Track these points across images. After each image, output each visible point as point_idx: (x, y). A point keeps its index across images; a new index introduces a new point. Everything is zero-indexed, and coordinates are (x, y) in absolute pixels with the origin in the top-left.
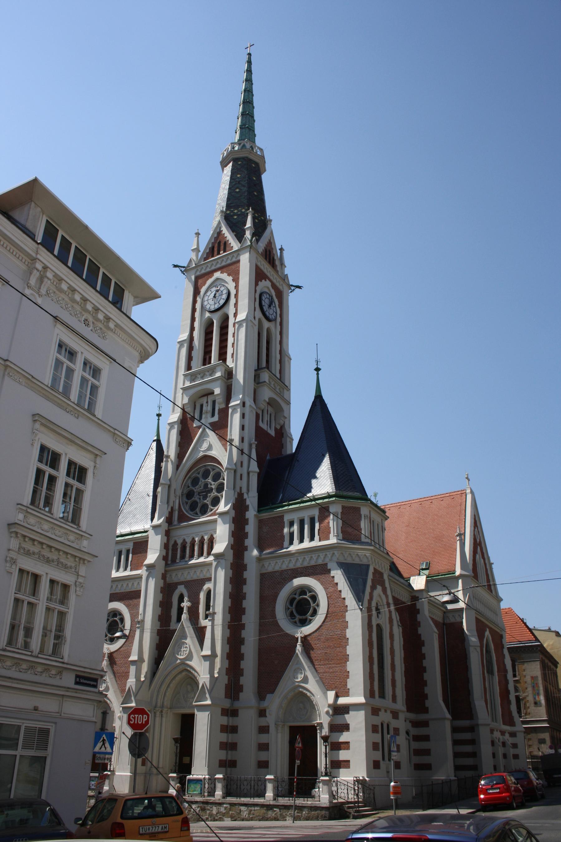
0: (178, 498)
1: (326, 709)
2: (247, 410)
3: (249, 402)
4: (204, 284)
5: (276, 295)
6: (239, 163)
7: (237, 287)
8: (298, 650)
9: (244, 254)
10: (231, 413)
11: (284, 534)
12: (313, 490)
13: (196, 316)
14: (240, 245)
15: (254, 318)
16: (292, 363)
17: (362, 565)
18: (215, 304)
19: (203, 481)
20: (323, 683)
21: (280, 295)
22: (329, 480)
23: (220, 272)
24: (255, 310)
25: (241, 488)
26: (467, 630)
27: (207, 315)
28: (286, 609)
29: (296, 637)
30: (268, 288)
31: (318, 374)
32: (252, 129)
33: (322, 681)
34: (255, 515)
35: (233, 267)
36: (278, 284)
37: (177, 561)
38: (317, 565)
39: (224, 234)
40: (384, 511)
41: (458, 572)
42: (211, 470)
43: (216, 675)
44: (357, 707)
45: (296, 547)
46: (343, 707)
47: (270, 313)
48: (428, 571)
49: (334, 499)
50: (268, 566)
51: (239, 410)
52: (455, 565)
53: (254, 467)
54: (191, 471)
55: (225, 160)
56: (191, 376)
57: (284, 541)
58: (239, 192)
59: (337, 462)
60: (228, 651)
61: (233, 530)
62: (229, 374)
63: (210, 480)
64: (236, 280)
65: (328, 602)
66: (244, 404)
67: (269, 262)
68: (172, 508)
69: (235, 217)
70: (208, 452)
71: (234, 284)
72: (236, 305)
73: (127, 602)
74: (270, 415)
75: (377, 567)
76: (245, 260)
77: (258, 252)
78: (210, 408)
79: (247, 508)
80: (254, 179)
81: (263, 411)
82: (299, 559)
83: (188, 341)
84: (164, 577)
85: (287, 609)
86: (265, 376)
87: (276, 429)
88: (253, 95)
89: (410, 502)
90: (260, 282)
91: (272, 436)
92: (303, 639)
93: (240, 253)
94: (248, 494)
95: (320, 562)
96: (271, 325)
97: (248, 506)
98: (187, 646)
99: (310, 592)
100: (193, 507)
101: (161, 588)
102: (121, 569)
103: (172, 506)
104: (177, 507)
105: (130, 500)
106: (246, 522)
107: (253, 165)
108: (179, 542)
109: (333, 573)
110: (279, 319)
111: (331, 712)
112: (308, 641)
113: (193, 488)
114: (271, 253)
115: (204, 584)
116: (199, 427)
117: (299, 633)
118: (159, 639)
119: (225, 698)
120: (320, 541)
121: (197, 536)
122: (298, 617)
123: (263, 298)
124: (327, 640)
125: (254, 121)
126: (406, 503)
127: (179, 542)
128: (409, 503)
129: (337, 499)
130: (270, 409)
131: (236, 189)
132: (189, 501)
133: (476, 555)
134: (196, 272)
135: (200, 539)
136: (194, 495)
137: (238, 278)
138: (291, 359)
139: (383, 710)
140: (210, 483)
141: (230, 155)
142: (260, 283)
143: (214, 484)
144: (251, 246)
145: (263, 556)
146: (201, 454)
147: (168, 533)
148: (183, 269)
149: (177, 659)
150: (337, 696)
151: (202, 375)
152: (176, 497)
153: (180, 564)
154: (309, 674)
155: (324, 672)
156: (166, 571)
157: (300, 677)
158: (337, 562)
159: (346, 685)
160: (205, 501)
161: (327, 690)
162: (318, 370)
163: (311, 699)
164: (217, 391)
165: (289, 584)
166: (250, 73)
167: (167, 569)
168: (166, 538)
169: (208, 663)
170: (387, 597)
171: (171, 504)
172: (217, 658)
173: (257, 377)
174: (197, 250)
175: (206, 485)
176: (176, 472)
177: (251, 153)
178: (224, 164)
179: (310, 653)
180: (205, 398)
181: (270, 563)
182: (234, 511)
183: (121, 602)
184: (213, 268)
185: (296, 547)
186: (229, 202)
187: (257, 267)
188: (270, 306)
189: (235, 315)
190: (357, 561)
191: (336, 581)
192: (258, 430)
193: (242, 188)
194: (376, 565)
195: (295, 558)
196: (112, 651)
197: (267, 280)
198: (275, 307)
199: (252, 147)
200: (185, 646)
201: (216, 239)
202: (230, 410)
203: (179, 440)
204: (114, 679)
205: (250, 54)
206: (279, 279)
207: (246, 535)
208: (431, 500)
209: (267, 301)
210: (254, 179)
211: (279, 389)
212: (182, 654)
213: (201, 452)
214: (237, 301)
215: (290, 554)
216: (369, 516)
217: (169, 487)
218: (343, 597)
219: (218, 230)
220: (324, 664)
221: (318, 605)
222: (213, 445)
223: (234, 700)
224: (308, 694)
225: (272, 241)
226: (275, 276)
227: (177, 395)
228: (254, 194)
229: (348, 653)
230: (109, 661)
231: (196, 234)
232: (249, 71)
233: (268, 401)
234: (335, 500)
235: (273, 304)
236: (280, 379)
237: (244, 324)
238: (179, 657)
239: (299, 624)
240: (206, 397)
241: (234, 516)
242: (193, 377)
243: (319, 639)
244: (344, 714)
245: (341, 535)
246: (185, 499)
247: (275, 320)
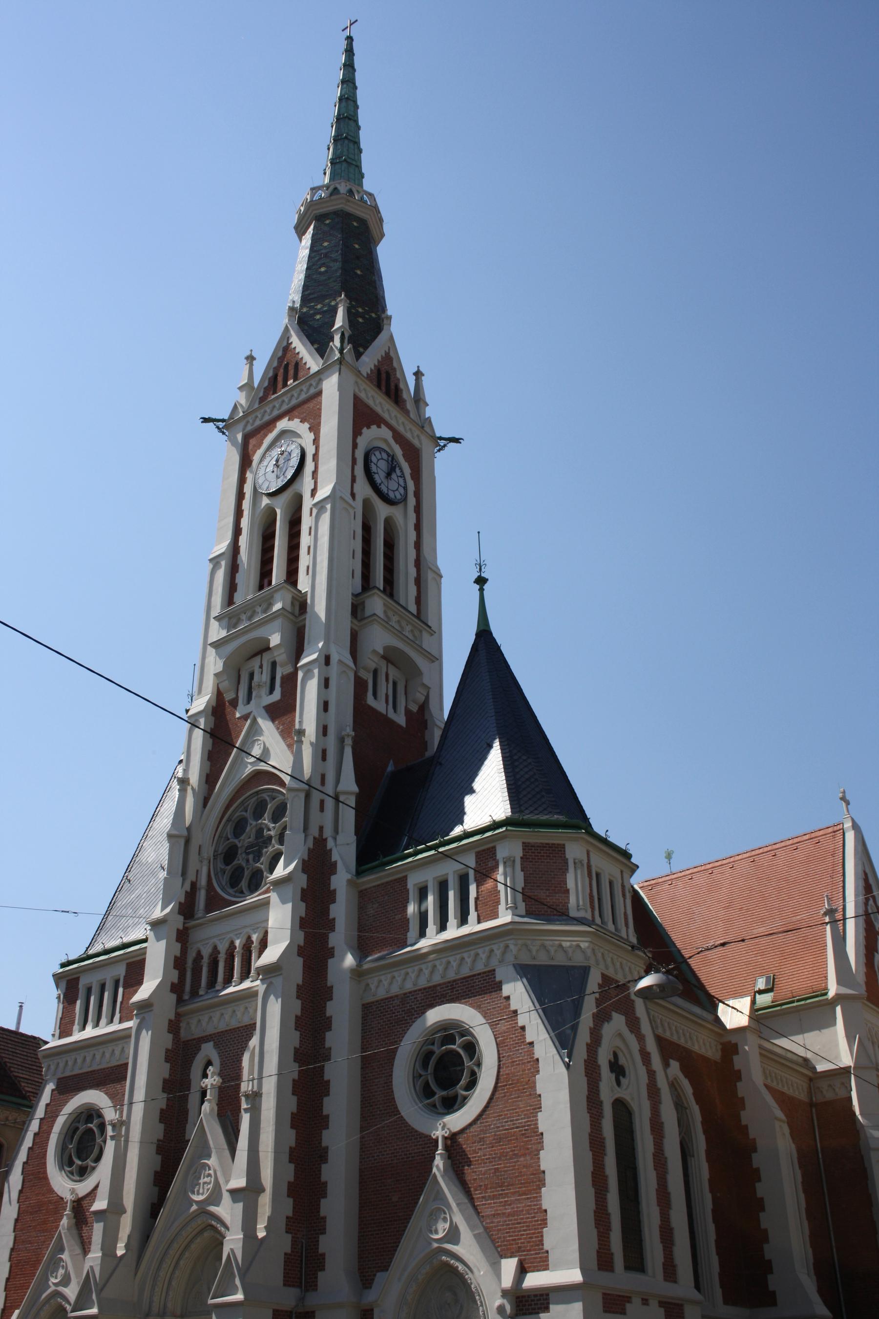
0: (205, 862)
1: (498, 1302)
2: (334, 671)
3: (341, 654)
4: (259, 445)
5: (404, 455)
6: (327, 222)
7: (316, 441)
8: (437, 1166)
9: (328, 377)
11: (408, 916)
12: (466, 818)
13: (244, 507)
14: (321, 362)
15: (353, 495)
16: (445, 583)
17: (574, 967)
18: (278, 477)
19: (254, 823)
20: (493, 1241)
21: (414, 456)
22: (500, 794)
23: (287, 418)
24: (353, 480)
25: (321, 828)
26: (861, 1114)
27: (265, 501)
28: (414, 1077)
29: (434, 1137)
30: (386, 441)
31: (481, 590)
32: (354, 163)
33: (490, 1236)
34: (349, 882)
35: (310, 405)
36: (408, 435)
37: (201, 992)
38: (474, 975)
39: (295, 348)
40: (627, 855)
41: (833, 989)
42: (268, 799)
43: (261, 1234)
44: (565, 1292)
45: (432, 939)
46: (535, 1296)
47: (391, 487)
48: (772, 994)
49: (504, 829)
50: (377, 987)
51: (316, 671)
52: (826, 978)
53: (349, 784)
54: (231, 806)
56: (230, 618)
57: (408, 930)
58: (326, 271)
59: (516, 757)
60: (292, 1179)
61: (303, 915)
62: (301, 605)
63: (266, 821)
64: (315, 429)
65: (499, 1054)
66: (327, 660)
67: (388, 393)
68: (194, 885)
69: (318, 317)
71: (312, 436)
72: (315, 473)
74: (395, 684)
75: (611, 973)
76: (331, 386)
77: (358, 373)
78: (265, 677)
79: (332, 868)
80: (357, 246)
81: (375, 672)
82: (438, 966)
83: (229, 556)
84: (174, 1027)
85: (416, 1077)
86: (376, 604)
87: (408, 712)
88: (357, 107)
89: (732, 859)
90: (365, 428)
91: (400, 726)
92: (449, 1142)
93: (322, 376)
94: (335, 839)
95: (480, 967)
96: (396, 512)
97: (336, 862)
98: (211, 1172)
99: (463, 1036)
100: (234, 880)
101: (167, 1051)
102: (103, 1021)
103: (194, 879)
104: (203, 881)
105: (129, 881)
106: (331, 896)
107: (355, 224)
108: (206, 952)
109: (507, 989)
110: (412, 501)
111: (508, 1308)
112: (460, 1145)
113: (236, 841)
114: (392, 377)
116: (245, 717)
117: (440, 1128)
118: (162, 1161)
119: (285, 1285)
120: (479, 922)
121: (238, 936)
122: (440, 1093)
123: (374, 459)
124: (499, 1139)
125: (360, 151)
126: (725, 862)
127: (206, 952)
128: (730, 863)
129: (509, 828)
130: (393, 672)
131: (320, 268)
132: (229, 867)
133: (873, 956)
134: (246, 426)
136: (237, 854)
137: (319, 424)
138: (441, 577)
139: (636, 1301)
140: (266, 825)
141: (310, 211)
142: (365, 430)
143: (274, 828)
144: (341, 361)
145: (366, 967)
146: (249, 769)
147: (182, 936)
148: (221, 424)
149: (191, 1202)
150: (522, 1271)
151: (249, 614)
152: (201, 862)
153: (205, 999)
154: (459, 1219)
155: (494, 1215)
156: (178, 1015)
157: (442, 1229)
158: (514, 965)
159: (541, 1243)
160: (258, 865)
161: (502, 1257)
162: (481, 581)
163: (466, 1280)
164: (275, 640)
165: (419, 1021)
166: (350, 69)
167: (181, 1010)
168: (179, 945)
169: (240, 1205)
170: (641, 1038)
171: (191, 876)
172: (262, 1195)
173: (357, 610)
174: (247, 386)
175: (260, 831)
176: (202, 812)
177: (349, 201)
178: (300, 231)
179: (463, 1173)
180: (258, 658)
181: (380, 981)
182: (305, 877)
183: (100, 1090)
184: (276, 413)
185: (432, 939)
186: (306, 293)
187: (357, 400)
188: (389, 475)
189: (314, 492)
190: (560, 960)
191: (513, 1008)
192: (362, 712)
193: (332, 264)
194: (607, 967)
195: (430, 965)
196: (81, 1194)
197: (383, 426)
198: (403, 476)
199: (351, 192)
201: (281, 359)
202: (300, 675)
203: (209, 747)
205: (350, 39)
206: (409, 426)
207: (331, 925)
208: (772, 851)
209: (383, 465)
210: (357, 246)
211: (412, 631)
212: (201, 1191)
213: (250, 767)
214: (316, 467)
215: (419, 957)
216: (585, 861)
217: (188, 841)
218: (528, 1040)
219: (285, 344)
220: (494, 1197)
221: (479, 1064)
222: (270, 749)
223: (307, 1290)
224: (461, 1267)
225: (392, 354)
226: (402, 419)
227: (207, 661)
228: (356, 274)
229: (542, 1168)
230: (75, 1217)
231: (247, 358)
232: (349, 66)
233: (381, 652)
234: (506, 830)
235: (397, 470)
236: (418, 616)
237: (329, 506)
239: (441, 1110)
240: (259, 656)
241: (305, 887)
242: (234, 621)
243: (482, 1140)
244: (538, 1313)
245: (522, 906)
246: (220, 865)
247: (405, 499)
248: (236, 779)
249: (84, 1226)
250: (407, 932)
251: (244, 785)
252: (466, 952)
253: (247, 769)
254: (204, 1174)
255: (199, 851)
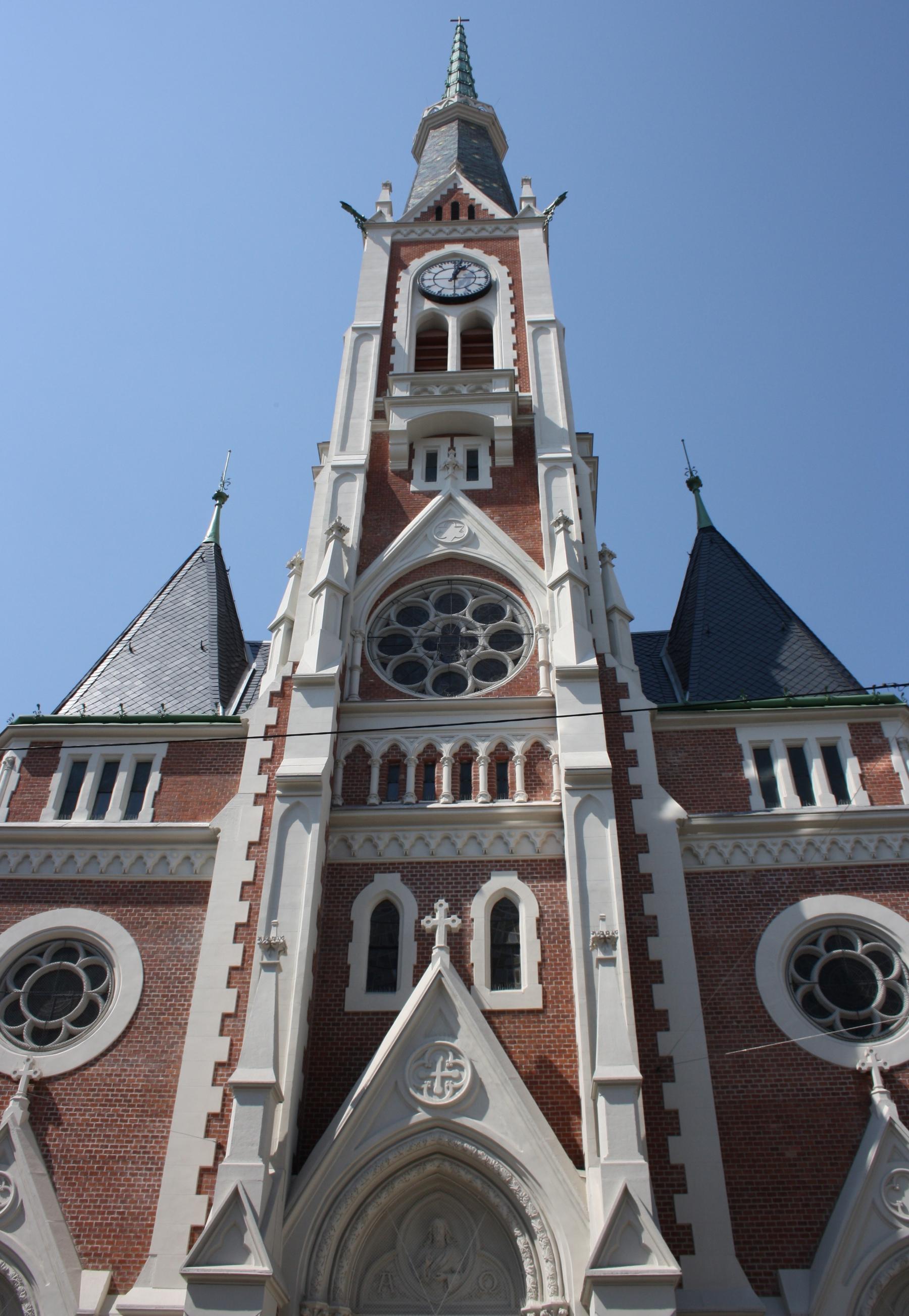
10: (546, 474)
13: (446, 246)
55: (448, 111)
70: (464, 548)
73: (134, 912)
113: (432, 612)
115: (486, 878)
135: (457, 749)
149: (413, 1106)
162: (694, 484)
183: (103, 912)
184: (455, 235)
196: (47, 1072)
200: (450, 1060)
204: (46, 1180)
219: (451, 186)
230: (31, 1108)
238: (425, 1098)
248: (413, 557)
249: (50, 1127)
250: (748, 795)
251: (425, 566)
252: (865, 833)
253: (437, 550)
254: (443, 1063)
255: (586, 564)
